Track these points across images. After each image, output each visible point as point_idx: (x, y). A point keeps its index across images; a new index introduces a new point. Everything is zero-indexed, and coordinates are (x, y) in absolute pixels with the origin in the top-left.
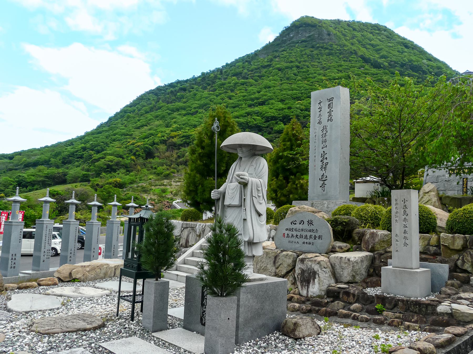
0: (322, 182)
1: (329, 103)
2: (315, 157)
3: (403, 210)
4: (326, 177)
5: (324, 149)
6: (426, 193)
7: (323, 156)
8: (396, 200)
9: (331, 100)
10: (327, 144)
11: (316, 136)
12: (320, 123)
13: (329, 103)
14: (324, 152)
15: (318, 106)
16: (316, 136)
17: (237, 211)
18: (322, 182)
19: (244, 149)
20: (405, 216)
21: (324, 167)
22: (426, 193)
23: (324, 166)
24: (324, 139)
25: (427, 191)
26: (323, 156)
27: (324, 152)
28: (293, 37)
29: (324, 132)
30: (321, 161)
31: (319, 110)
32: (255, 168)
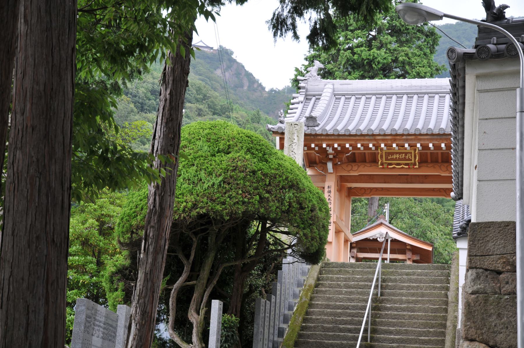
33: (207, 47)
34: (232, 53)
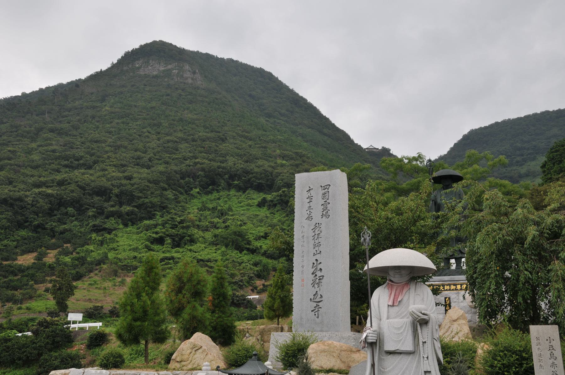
0: (315, 304)
1: (324, 191)
2: (303, 267)
3: (549, 352)
4: (321, 296)
5: (317, 257)
6: (454, 321)
7: (316, 266)
8: (538, 339)
9: (326, 187)
10: (321, 249)
11: (303, 236)
12: (310, 218)
13: (324, 191)
14: (316, 260)
15: (306, 195)
16: (303, 236)
17: (405, 360)
18: (315, 304)
19: (403, 272)
20: (552, 360)
21: (318, 281)
22: (454, 321)
23: (317, 281)
24: (317, 241)
25: (455, 317)
26: (316, 266)
27: (316, 260)
28: (139, 68)
29: (317, 232)
30: (313, 274)
31: (308, 200)
32: (423, 299)
33: (375, 148)
34: (390, 150)
